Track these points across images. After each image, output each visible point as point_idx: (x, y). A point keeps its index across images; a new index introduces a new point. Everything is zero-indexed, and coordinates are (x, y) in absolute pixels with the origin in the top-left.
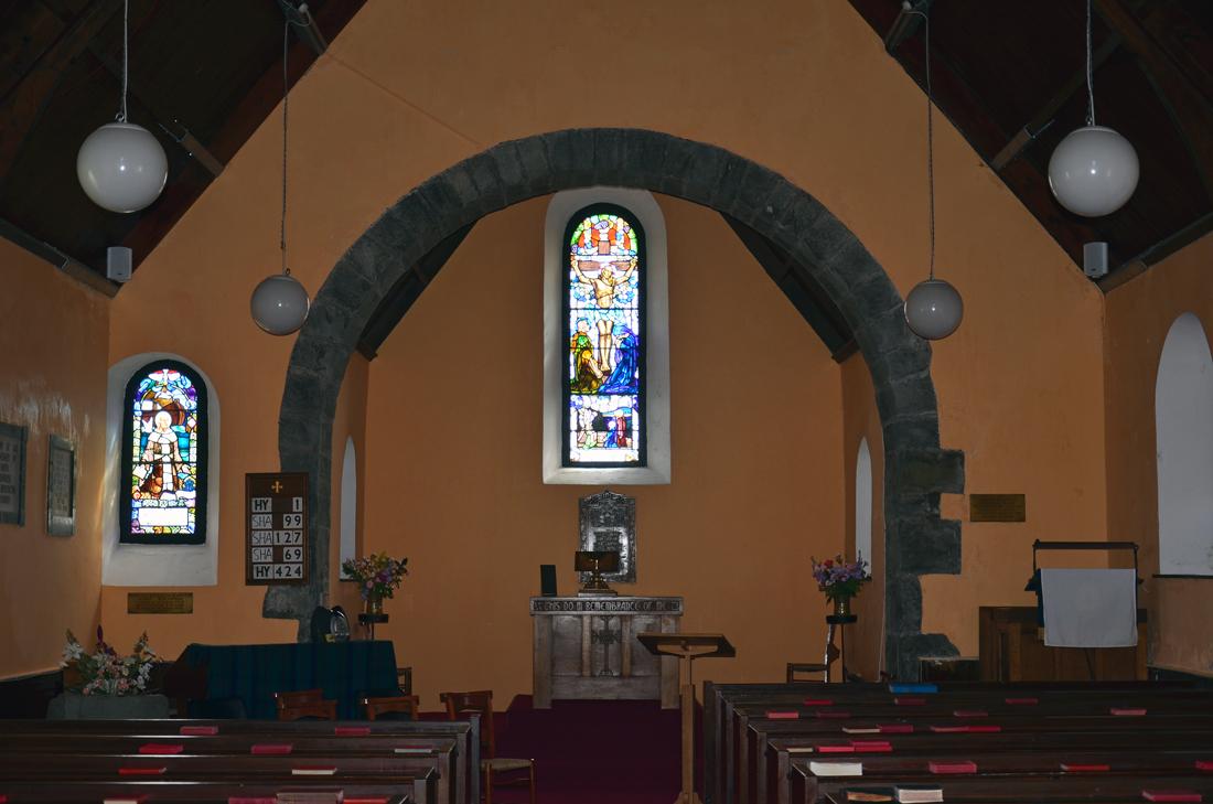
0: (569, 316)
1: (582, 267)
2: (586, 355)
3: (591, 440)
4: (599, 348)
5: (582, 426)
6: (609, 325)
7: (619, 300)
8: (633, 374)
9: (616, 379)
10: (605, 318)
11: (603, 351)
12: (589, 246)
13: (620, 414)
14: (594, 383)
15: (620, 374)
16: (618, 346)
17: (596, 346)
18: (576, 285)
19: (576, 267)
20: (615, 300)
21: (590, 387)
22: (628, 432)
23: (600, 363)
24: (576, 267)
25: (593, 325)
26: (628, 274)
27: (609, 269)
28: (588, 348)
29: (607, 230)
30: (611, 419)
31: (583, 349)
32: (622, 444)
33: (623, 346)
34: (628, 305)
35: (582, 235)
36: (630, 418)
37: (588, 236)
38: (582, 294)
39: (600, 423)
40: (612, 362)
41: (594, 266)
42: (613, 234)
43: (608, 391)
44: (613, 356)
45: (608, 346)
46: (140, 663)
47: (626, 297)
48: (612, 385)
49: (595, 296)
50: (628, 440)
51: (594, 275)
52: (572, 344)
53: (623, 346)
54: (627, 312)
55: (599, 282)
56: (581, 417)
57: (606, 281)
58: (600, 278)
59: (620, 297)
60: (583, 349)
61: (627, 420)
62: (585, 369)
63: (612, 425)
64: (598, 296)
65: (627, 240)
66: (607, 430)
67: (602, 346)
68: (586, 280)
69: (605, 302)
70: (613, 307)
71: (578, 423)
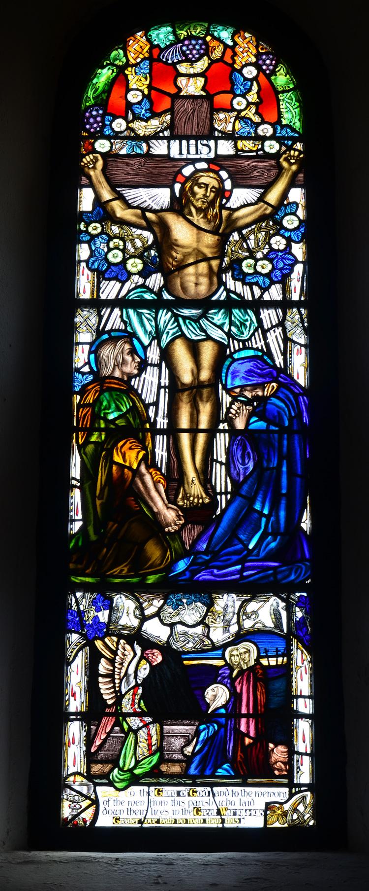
0: (83, 514)
1: (119, 174)
2: (129, 455)
3: (137, 752)
4: (173, 431)
5: (108, 696)
6: (208, 352)
7: (241, 277)
8: (294, 519)
9: (233, 534)
10: (192, 333)
11: (185, 438)
12: (142, 111)
13: (245, 655)
14: (153, 551)
15: (246, 520)
16: (240, 424)
17: (162, 422)
18: (95, 228)
19: (96, 174)
20: (228, 278)
21: (139, 564)
22: (277, 721)
23: (174, 479)
24: (96, 174)
25: (154, 355)
26: (273, 197)
27: (208, 179)
28: (137, 428)
29: (202, 65)
30: (211, 675)
31: (116, 434)
32: (253, 769)
33: (258, 424)
34: (275, 293)
35: (120, 79)
36: (286, 672)
37: (138, 84)
38: (115, 257)
39: (175, 686)
40: (210, 466)
41: (161, 172)
42: (221, 78)
43: (204, 576)
44: (220, 453)
45: (204, 424)
46: (178, 40)
47: (265, 267)
48: (216, 557)
49: (162, 256)
50: (279, 753)
51: (161, 197)
52: (79, 415)
53: (258, 424)
54: (269, 316)
55: (172, 220)
56: (103, 667)
57: (198, 219)
58: (179, 206)
59: (247, 266)
60: (116, 434)
61: (273, 682)
62: (119, 500)
63: (217, 696)
64: (171, 263)
65: (269, 98)
66: (197, 711)
67: (184, 422)
68: (127, 214)
69: (195, 281)
70: (221, 295)
71: (92, 688)
